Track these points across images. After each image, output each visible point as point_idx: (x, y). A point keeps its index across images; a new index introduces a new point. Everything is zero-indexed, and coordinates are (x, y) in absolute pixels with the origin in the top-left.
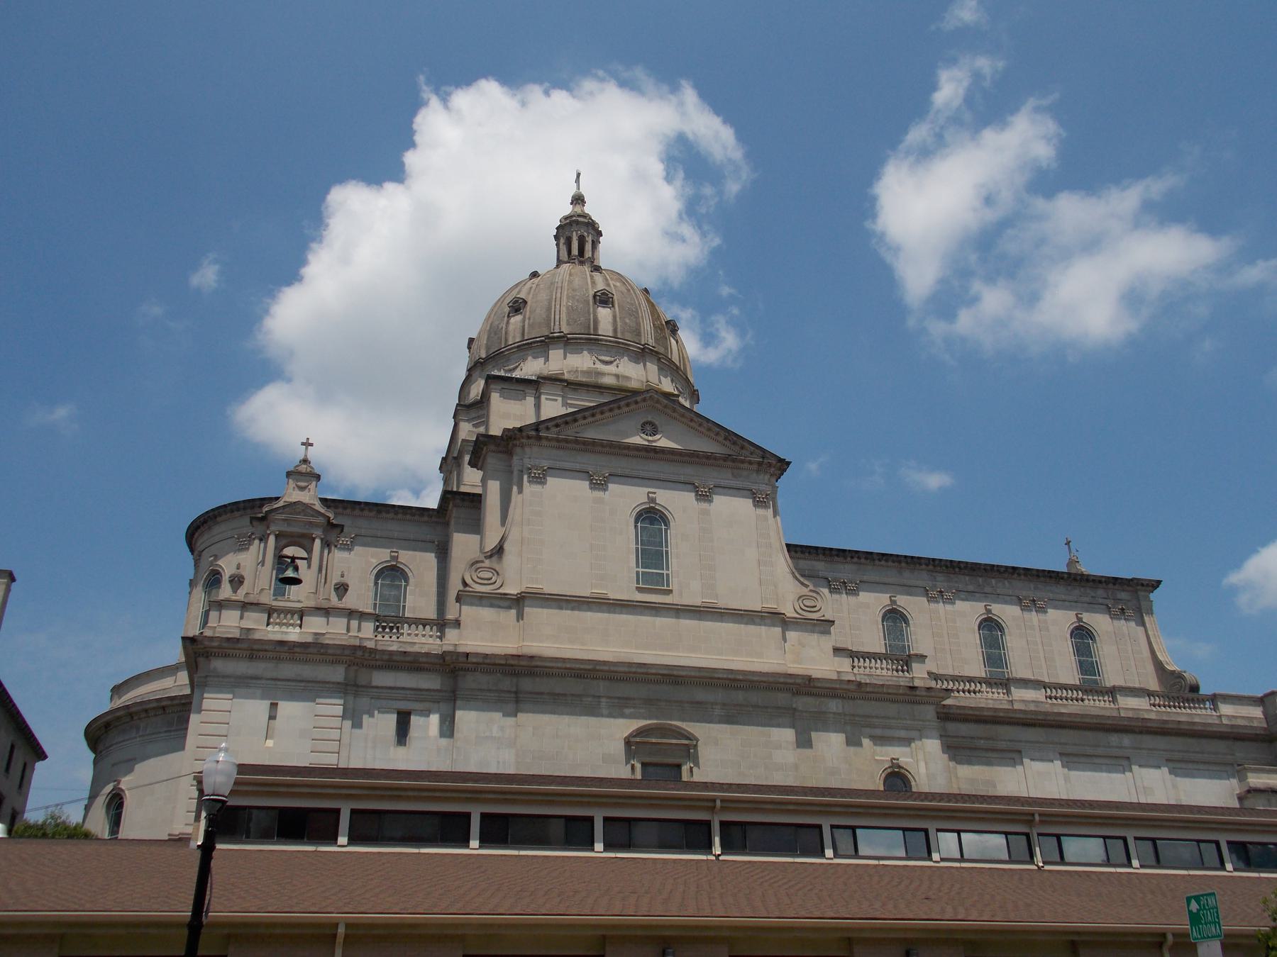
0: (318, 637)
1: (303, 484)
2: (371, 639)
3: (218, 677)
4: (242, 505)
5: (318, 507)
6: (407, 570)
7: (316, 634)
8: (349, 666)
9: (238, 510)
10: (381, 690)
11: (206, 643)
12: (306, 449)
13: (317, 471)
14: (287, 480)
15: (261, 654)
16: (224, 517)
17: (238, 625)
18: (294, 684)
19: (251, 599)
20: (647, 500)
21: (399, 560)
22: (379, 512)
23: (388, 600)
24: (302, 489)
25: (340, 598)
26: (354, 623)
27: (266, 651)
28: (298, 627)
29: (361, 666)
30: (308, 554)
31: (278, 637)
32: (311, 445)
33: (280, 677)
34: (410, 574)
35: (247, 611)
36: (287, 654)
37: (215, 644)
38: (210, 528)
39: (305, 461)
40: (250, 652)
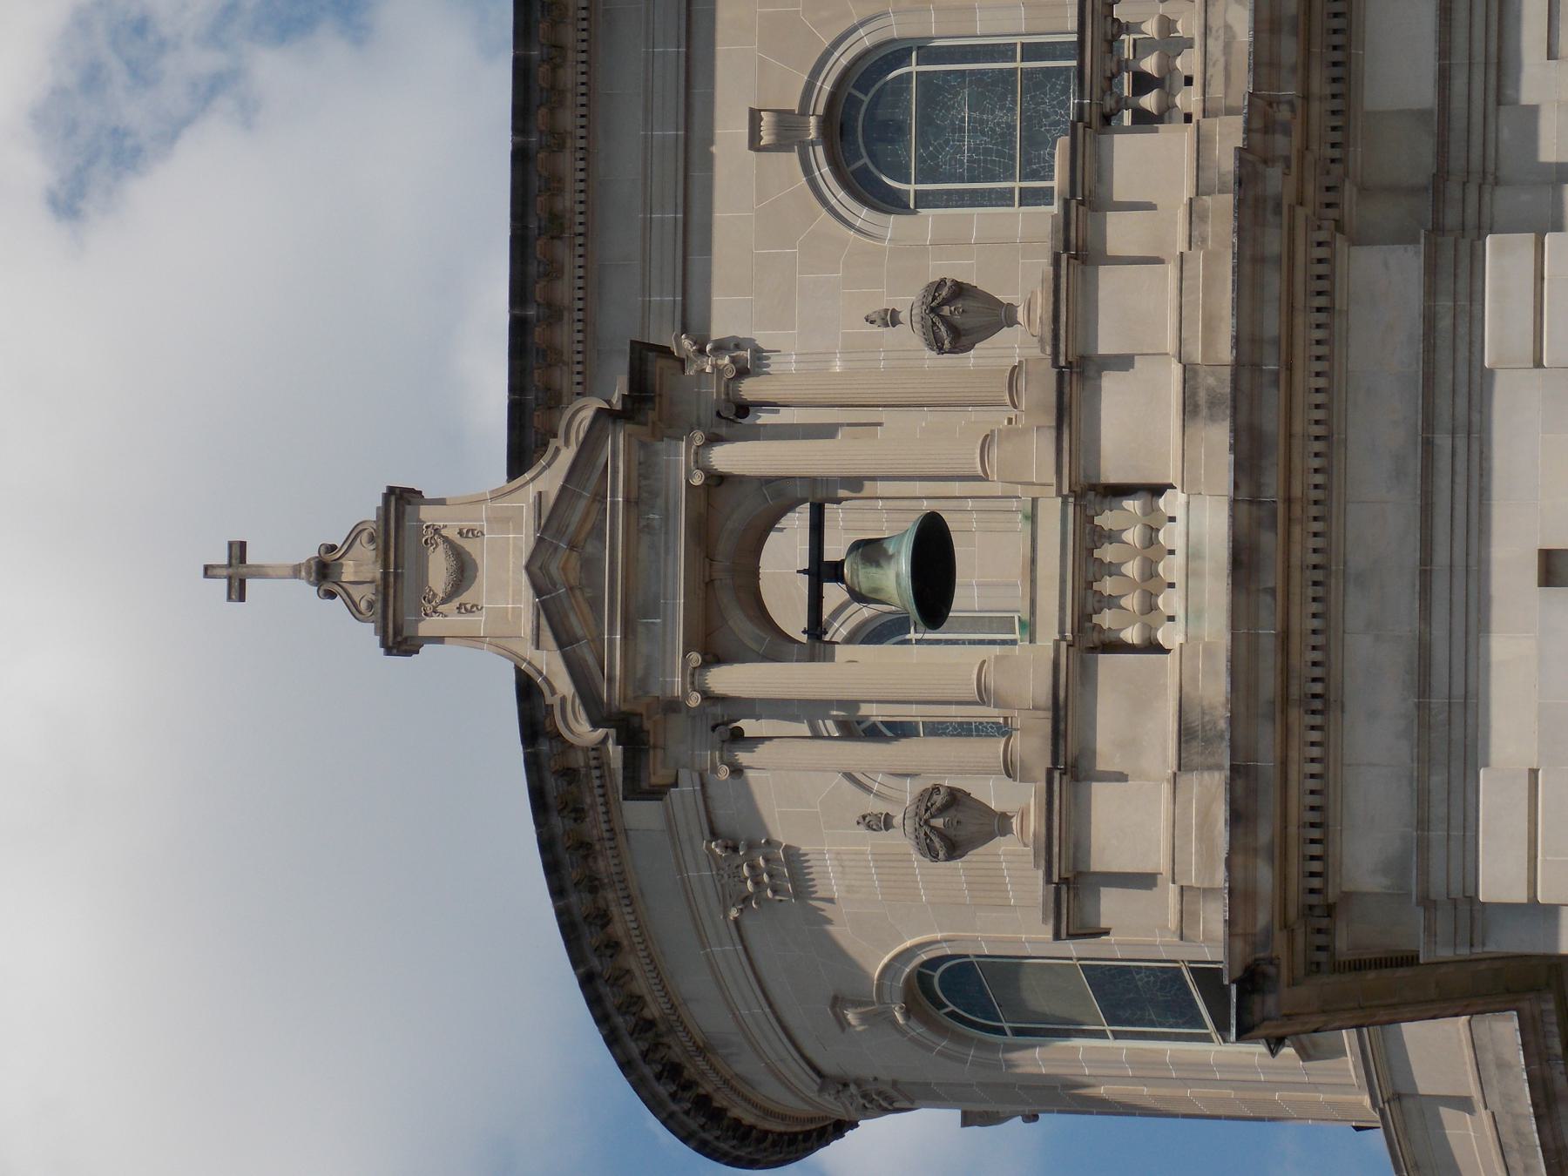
0: (1202, 397)
1: (439, 570)
2: (1201, 142)
3: (1423, 846)
4: (573, 899)
5: (549, 478)
6: (841, 59)
7: (1189, 409)
8: (1339, 226)
9: (602, 918)
10: (1459, 57)
11: (1263, 919)
12: (261, 572)
13: (369, 508)
14: (426, 649)
15: (1302, 657)
16: (642, 984)
17: (1166, 788)
18: (1443, 483)
19: (1032, 745)
20: (794, 157)
21: (794, 105)
22: (555, 225)
23: (1006, 137)
24: (463, 571)
25: (1000, 316)
26: (1121, 232)
27: (1285, 637)
28: (1161, 502)
29: (1337, 169)
30: (791, 507)
31: (1216, 589)
32: (238, 551)
33: (1412, 555)
34: (865, 39)
35: (1092, 754)
36: (1297, 531)
37: (1265, 876)
38: (703, 1050)
39: (324, 572)
40: (1295, 714)
